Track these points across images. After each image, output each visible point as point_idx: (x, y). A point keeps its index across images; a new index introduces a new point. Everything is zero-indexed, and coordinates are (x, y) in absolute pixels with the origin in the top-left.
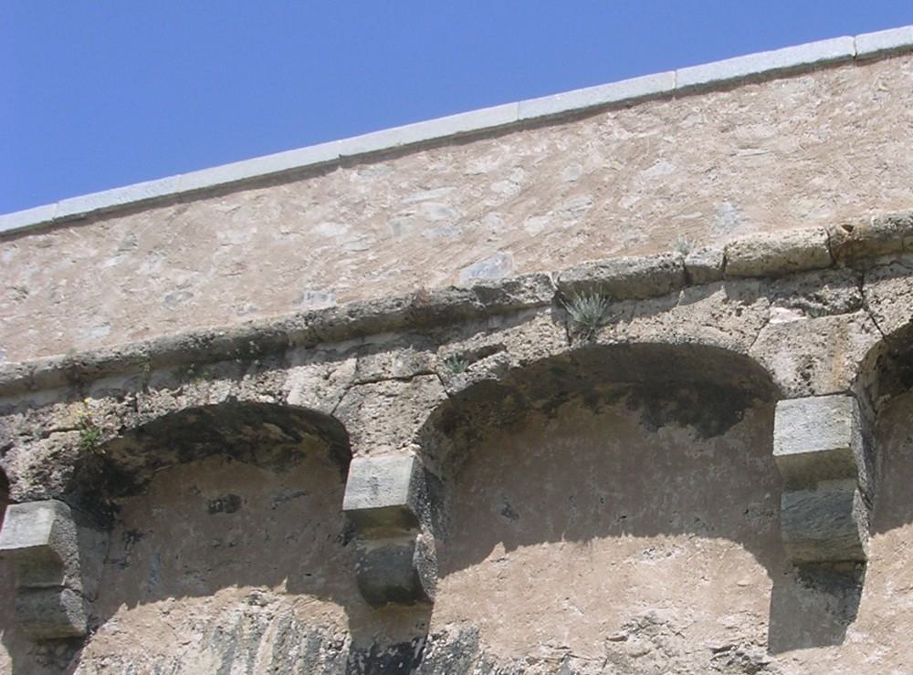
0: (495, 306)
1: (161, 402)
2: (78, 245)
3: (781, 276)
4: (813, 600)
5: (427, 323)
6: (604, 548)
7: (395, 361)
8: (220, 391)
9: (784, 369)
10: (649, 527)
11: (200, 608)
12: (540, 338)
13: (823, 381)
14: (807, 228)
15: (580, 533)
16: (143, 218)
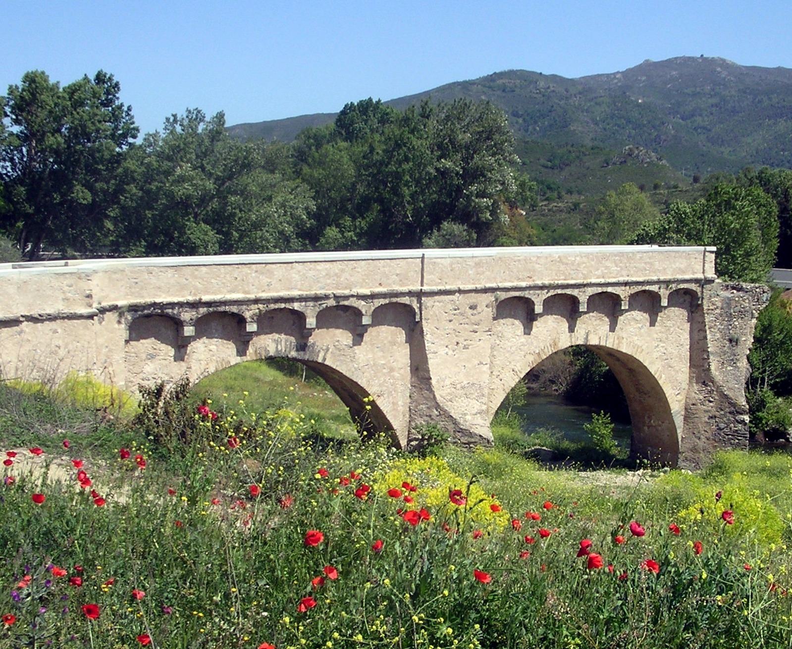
0: (326, 297)
1: (272, 306)
2: (245, 269)
3: (363, 297)
4: (358, 338)
5: (316, 299)
6: (330, 330)
7: (311, 304)
8: (283, 306)
9: (364, 312)
10: (338, 327)
11: (270, 336)
12: (332, 302)
13: (368, 314)
14: (367, 291)
15: (328, 328)
16: (258, 265)
